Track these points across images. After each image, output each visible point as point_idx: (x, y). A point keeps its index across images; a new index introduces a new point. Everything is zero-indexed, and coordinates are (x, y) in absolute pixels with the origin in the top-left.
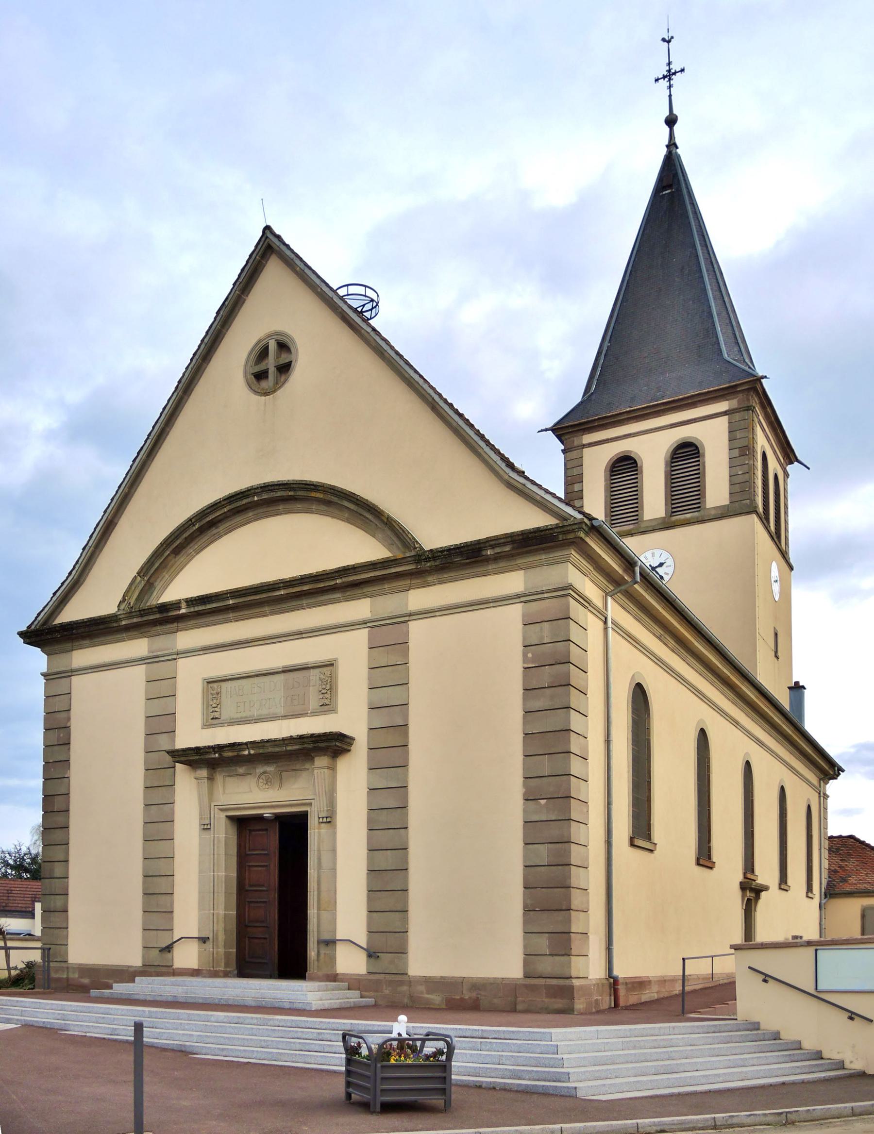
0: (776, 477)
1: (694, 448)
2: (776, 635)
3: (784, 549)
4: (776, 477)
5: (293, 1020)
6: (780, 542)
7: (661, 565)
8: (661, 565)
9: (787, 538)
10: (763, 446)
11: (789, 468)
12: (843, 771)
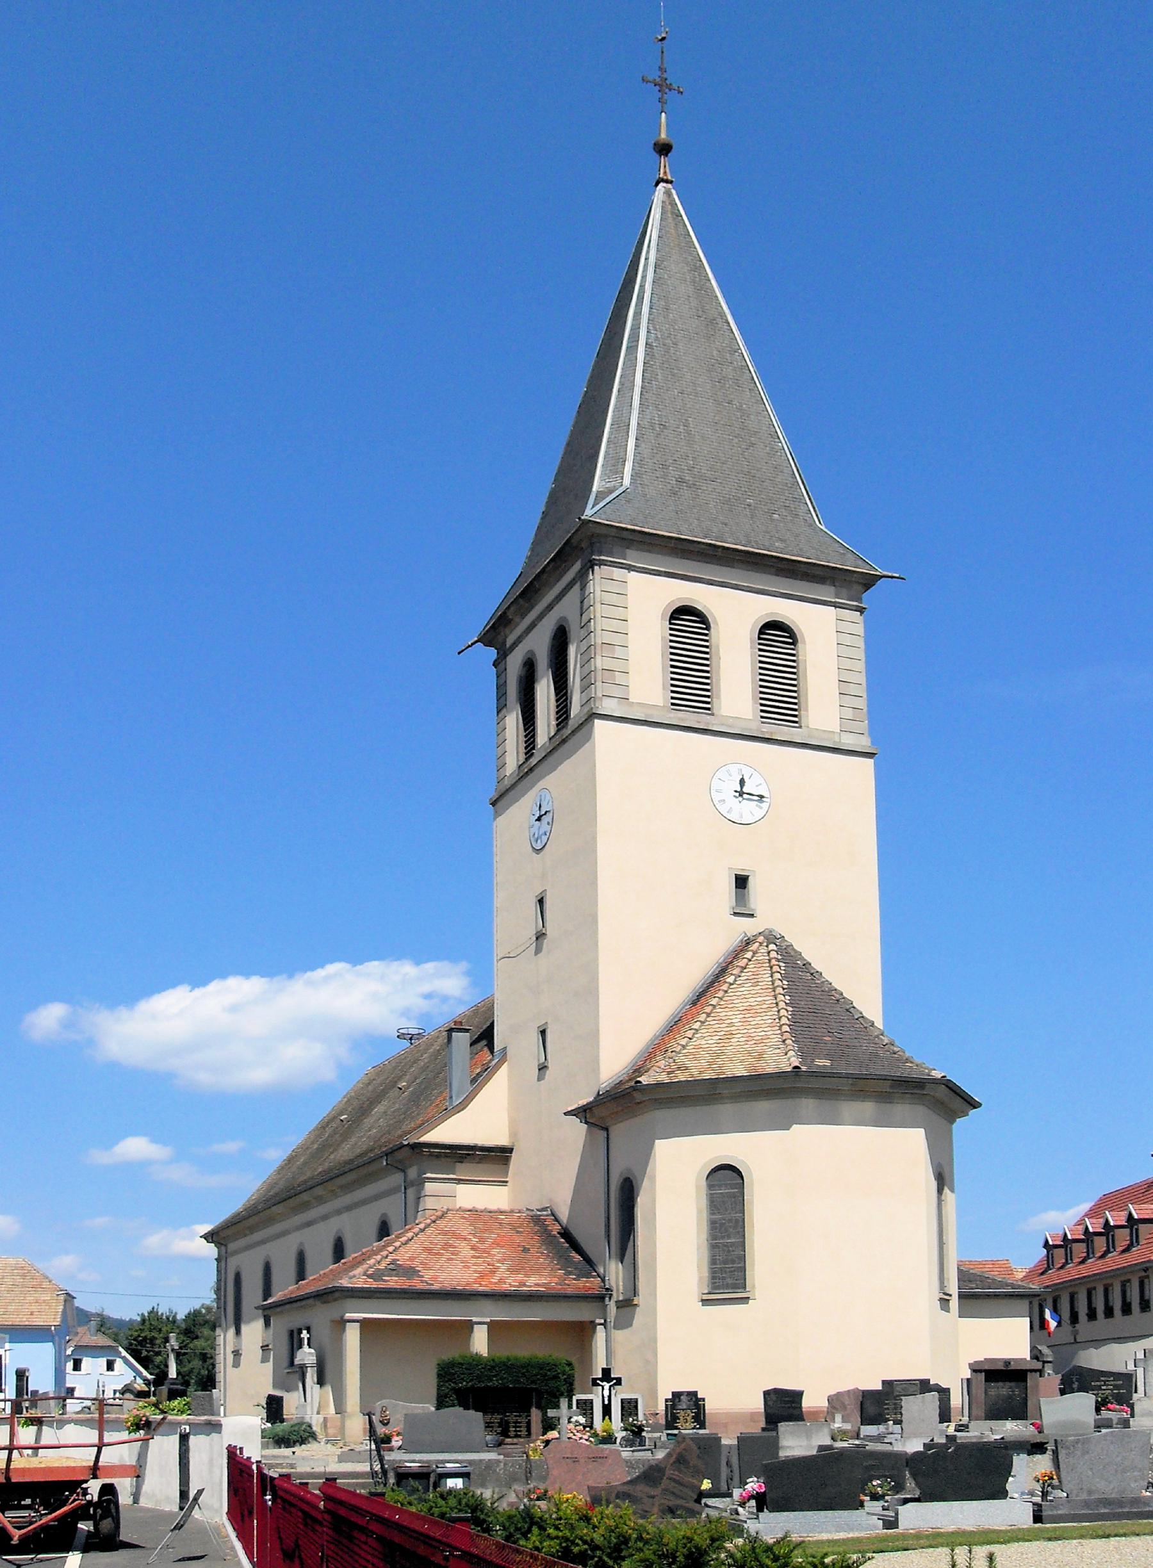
7: (742, 782)
8: (742, 782)
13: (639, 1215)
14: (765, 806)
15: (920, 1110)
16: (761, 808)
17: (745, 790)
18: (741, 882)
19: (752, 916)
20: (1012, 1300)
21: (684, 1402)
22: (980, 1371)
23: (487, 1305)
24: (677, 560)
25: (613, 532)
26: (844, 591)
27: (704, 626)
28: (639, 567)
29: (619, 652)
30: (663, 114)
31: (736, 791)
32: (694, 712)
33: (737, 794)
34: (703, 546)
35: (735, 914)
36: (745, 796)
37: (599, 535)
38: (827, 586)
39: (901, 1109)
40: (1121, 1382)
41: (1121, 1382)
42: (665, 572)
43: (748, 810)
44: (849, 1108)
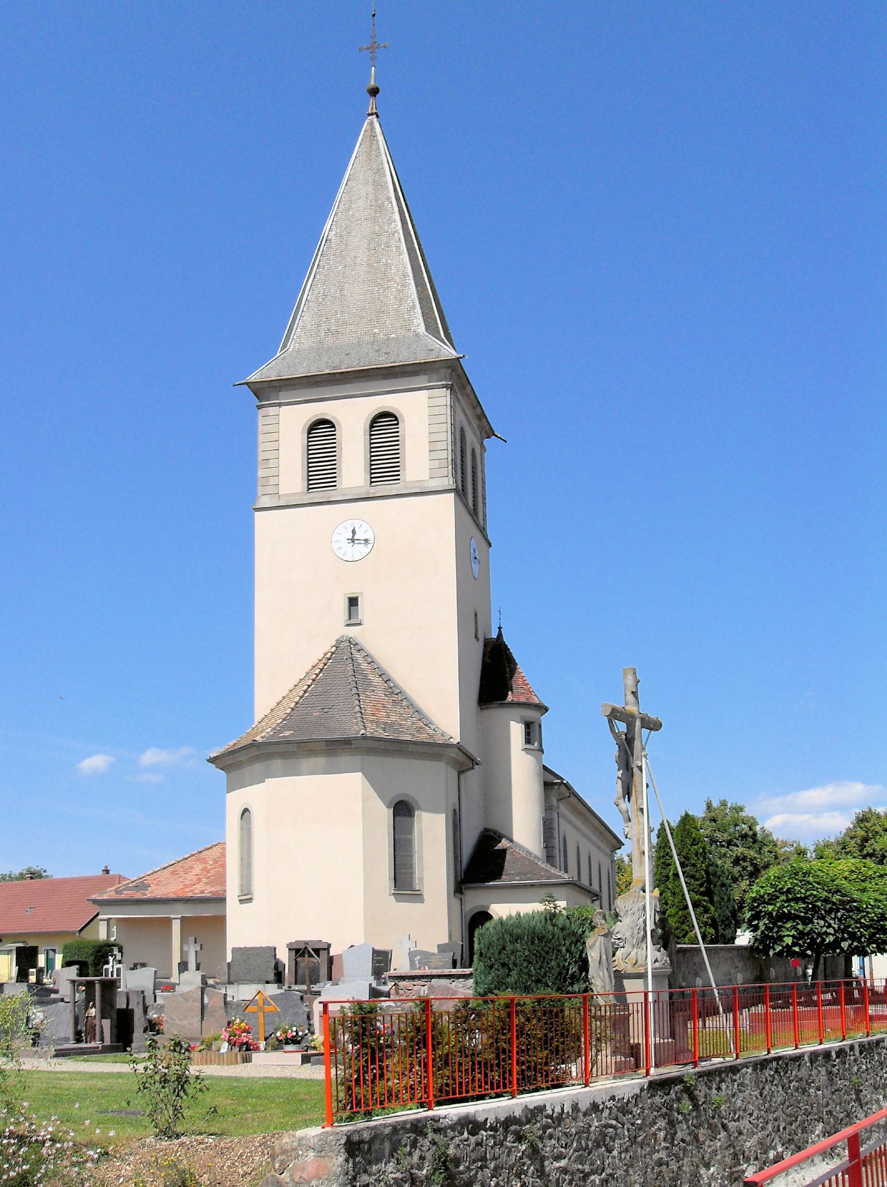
0: (473, 451)
1: (394, 419)
2: (476, 615)
3: (482, 525)
4: (473, 451)
5: (665, 830)
6: (477, 518)
7: (354, 532)
8: (354, 532)
9: (485, 515)
10: (461, 421)
11: (486, 442)
12: (623, 845)
13: (416, 831)
14: (370, 546)
15: (357, 759)
16: (368, 547)
17: (355, 538)
18: (353, 602)
19: (360, 624)
20: (558, 888)
21: (468, 963)
22: (293, 949)
23: (180, 907)
24: (310, 390)
25: (266, 385)
26: (435, 376)
27: (394, 419)
28: (286, 403)
29: (272, 463)
30: (373, 68)
31: (348, 539)
32: (323, 491)
33: (350, 541)
34: (326, 376)
35: (348, 625)
36: (356, 542)
37: (259, 389)
38: (421, 376)
39: (345, 759)
40: (381, 958)
41: (381, 958)
42: (304, 400)
43: (360, 550)
44: (307, 763)
